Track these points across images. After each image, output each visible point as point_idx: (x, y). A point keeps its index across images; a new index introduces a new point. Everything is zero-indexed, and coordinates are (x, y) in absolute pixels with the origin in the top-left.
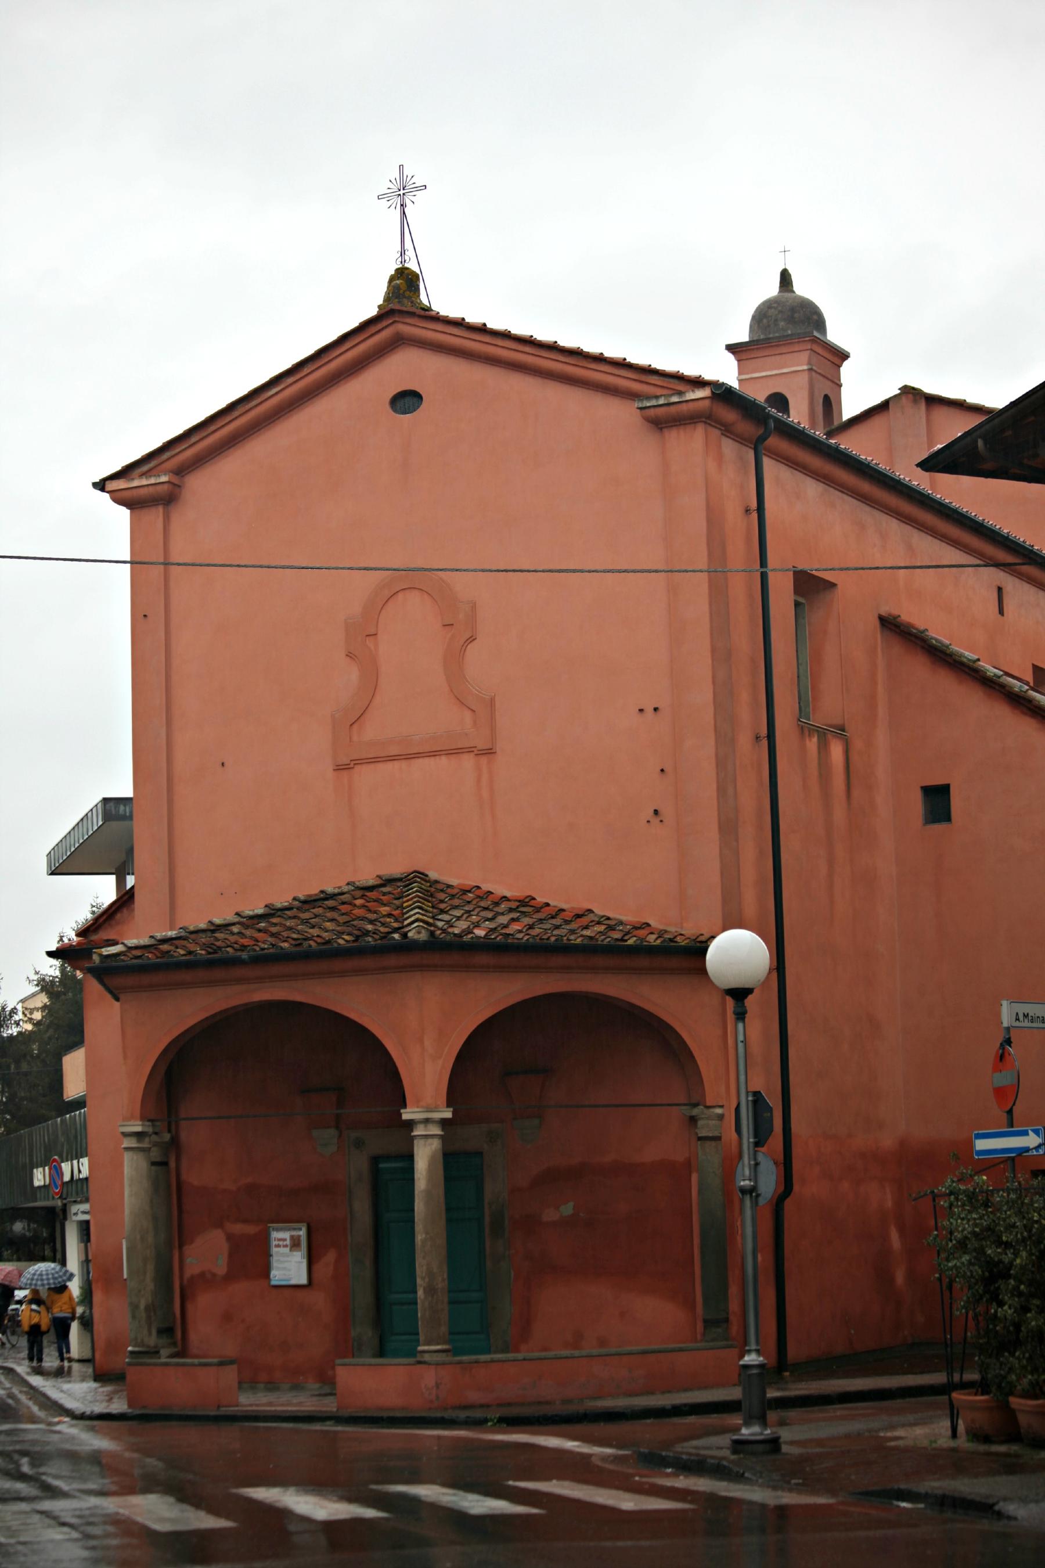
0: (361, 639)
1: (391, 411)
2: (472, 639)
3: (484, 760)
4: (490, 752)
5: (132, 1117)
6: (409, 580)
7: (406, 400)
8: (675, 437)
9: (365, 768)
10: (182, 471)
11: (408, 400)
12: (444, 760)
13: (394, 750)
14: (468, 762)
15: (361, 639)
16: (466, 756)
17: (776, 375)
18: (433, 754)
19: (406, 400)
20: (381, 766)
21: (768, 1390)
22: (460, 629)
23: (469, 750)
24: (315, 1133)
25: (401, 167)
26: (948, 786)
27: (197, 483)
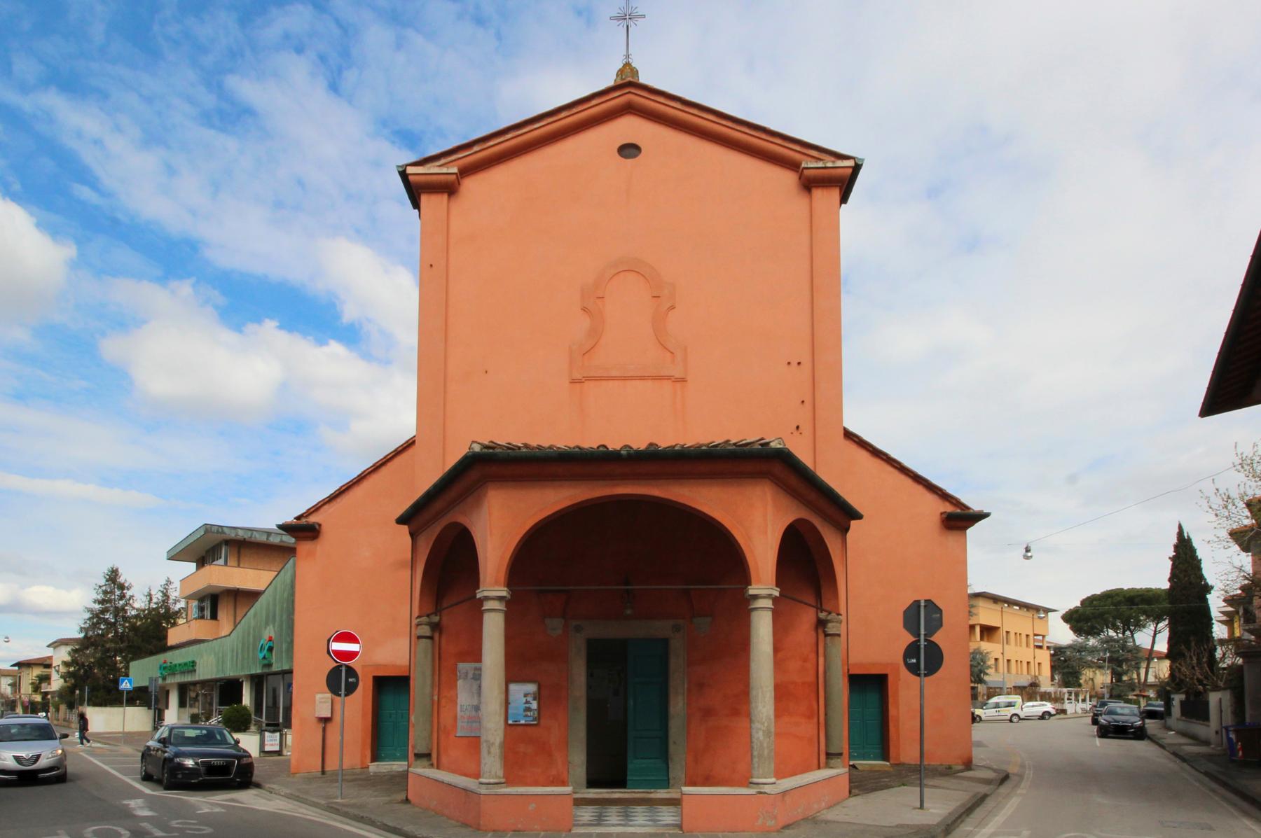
0: (592, 302)
1: (629, 161)
2: (672, 308)
3: (678, 385)
4: (683, 380)
5: (497, 583)
6: (631, 268)
7: (629, 150)
8: (818, 194)
9: (592, 384)
10: (466, 171)
11: (633, 151)
12: (649, 383)
13: (614, 373)
14: (667, 385)
15: (592, 302)
16: (665, 382)
17: (825, 692)
18: (642, 378)
19: (629, 150)
20: (604, 383)
21: (531, 688)
22: (663, 299)
23: (668, 378)
24: (548, 621)
25: (644, 16)
26: (375, 678)
27: (471, 185)
